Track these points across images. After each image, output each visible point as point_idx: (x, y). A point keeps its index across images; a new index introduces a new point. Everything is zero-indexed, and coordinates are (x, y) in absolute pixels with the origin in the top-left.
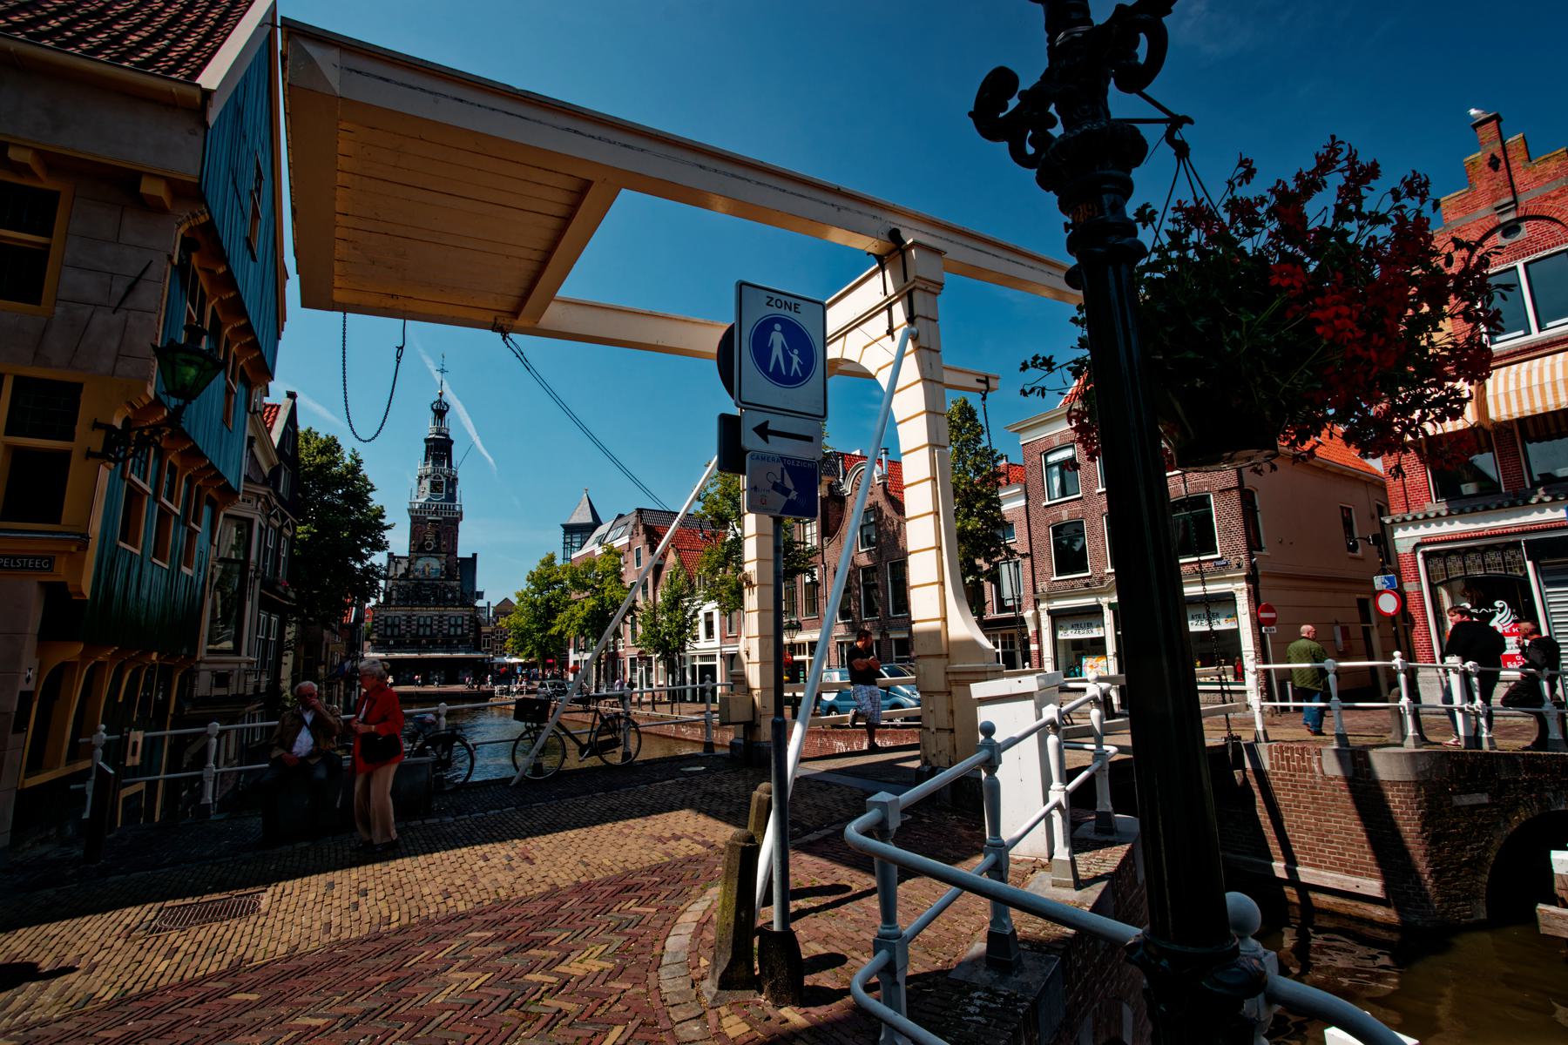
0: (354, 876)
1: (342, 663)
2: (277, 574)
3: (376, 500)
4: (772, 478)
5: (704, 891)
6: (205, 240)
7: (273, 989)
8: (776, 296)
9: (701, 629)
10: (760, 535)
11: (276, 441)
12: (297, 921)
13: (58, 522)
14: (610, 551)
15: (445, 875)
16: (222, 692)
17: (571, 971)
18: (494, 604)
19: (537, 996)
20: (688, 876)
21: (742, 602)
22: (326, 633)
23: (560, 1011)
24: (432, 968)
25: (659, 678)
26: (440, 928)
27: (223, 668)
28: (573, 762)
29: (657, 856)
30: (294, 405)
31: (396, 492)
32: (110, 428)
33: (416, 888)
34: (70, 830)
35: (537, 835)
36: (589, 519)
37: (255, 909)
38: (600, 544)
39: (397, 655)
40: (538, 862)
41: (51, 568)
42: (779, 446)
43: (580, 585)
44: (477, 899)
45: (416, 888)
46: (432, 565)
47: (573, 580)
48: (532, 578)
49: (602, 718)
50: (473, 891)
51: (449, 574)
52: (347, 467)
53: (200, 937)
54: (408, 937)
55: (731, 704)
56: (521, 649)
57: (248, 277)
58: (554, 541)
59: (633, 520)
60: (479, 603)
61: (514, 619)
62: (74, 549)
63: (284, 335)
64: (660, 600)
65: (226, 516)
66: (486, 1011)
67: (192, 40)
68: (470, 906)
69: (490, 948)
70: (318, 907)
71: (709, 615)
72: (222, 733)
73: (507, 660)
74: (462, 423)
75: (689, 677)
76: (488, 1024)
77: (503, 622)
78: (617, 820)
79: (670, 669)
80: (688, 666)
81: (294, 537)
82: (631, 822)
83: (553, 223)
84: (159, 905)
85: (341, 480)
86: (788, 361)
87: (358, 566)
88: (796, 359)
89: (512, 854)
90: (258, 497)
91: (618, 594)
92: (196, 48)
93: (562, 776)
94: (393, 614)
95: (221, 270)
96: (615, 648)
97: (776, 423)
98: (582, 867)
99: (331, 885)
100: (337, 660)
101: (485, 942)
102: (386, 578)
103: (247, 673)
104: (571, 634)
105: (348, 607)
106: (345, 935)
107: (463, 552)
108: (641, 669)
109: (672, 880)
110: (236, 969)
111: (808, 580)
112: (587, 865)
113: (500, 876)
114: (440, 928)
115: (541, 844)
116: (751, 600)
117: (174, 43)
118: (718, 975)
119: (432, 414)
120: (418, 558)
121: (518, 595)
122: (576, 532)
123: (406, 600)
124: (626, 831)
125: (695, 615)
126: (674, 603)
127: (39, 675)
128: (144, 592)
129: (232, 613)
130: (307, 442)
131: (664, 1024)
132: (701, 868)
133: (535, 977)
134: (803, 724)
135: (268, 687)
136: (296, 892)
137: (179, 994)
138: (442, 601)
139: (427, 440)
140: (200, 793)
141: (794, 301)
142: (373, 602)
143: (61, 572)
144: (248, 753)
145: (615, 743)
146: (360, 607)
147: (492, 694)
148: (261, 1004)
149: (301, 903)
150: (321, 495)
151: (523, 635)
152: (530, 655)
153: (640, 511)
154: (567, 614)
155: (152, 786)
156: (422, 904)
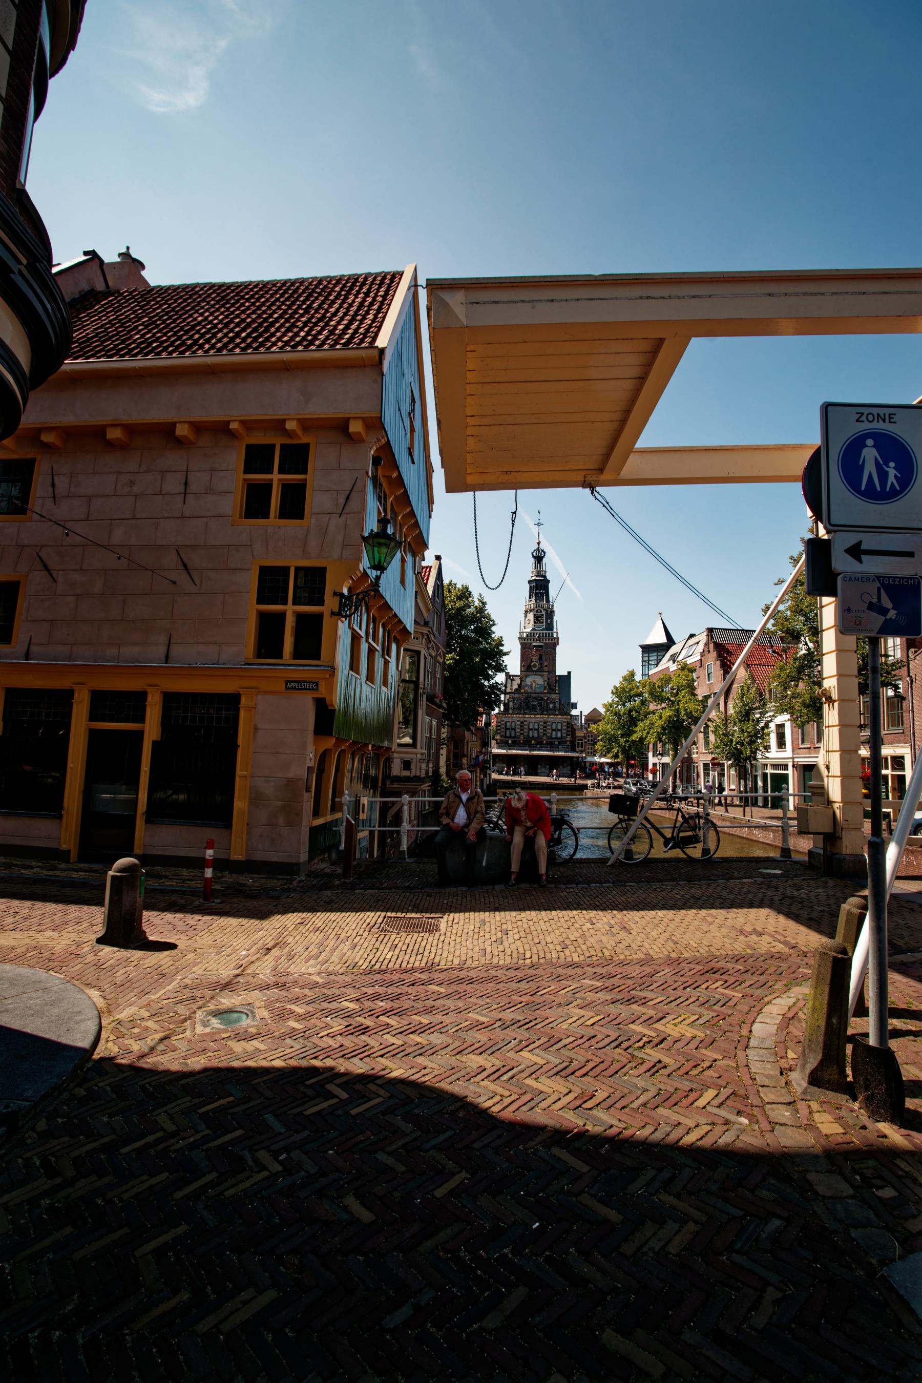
0: (498, 918)
1: (477, 757)
2: (435, 690)
3: (497, 632)
4: (867, 599)
5: (788, 987)
6: (385, 457)
7: (454, 987)
8: (866, 411)
9: (773, 739)
10: (840, 651)
11: (430, 593)
12: (464, 943)
13: (319, 659)
14: (684, 667)
15: (562, 930)
16: (406, 773)
17: (668, 1031)
18: (585, 713)
19: (640, 1044)
20: (771, 970)
21: (820, 717)
22: (467, 734)
23: (660, 1062)
24: (559, 1000)
25: (731, 785)
26: (561, 971)
27: (407, 757)
28: (660, 851)
29: (740, 946)
30: (440, 564)
31: (510, 624)
32: (341, 595)
33: (541, 936)
34: (334, 856)
35: (632, 909)
36: (663, 639)
37: (437, 929)
38: (674, 661)
39: (514, 752)
40: (634, 932)
41: (317, 690)
42: (872, 566)
43: (658, 697)
44: (587, 954)
45: (541, 936)
46: (537, 681)
47: (651, 694)
48: (616, 692)
49: (683, 816)
50: (584, 947)
51: (550, 688)
52: (476, 608)
53: (408, 941)
54: (539, 972)
55: (811, 816)
56: (609, 751)
57: (411, 475)
58: (634, 662)
59: (703, 638)
60: (574, 712)
61: (601, 726)
62: (328, 676)
63: (433, 514)
64: (731, 711)
65: (405, 650)
66: (600, 1045)
67: (371, 317)
68: (582, 958)
69: (600, 995)
70: (476, 936)
71: (780, 727)
72: (410, 802)
73: (597, 759)
74: (554, 568)
75: (760, 784)
76: (603, 1056)
77: (593, 728)
78: (701, 907)
79: (742, 775)
80: (759, 773)
81: (444, 662)
82: (713, 912)
83: (629, 385)
84: (383, 914)
85: (473, 619)
86: (883, 476)
87: (486, 683)
88: (892, 473)
89: (612, 922)
90: (423, 634)
91: (691, 706)
92: (373, 321)
93: (648, 862)
94: (510, 720)
95: (395, 475)
96: (690, 754)
97: (870, 541)
98: (671, 944)
99: (484, 922)
100: (474, 755)
101: (597, 990)
102: (505, 693)
103: (421, 761)
104: (651, 739)
105: (481, 714)
106: (495, 961)
107: (560, 671)
108: (714, 774)
109: (759, 972)
110: (430, 968)
111: (891, 693)
112: (676, 943)
113: (604, 939)
114: (561, 971)
115: (636, 918)
116: (831, 715)
117: (361, 322)
118: (808, 1071)
119: (533, 560)
120: (527, 676)
121: (605, 706)
122: (652, 651)
123: (519, 709)
124: (709, 919)
125: (767, 726)
126: (746, 715)
127: (315, 756)
128: (363, 704)
129: (410, 720)
130: (450, 592)
131: (756, 1101)
132: (784, 965)
133: (637, 1028)
134: (899, 844)
135: (433, 772)
136: (461, 923)
137: (400, 976)
138: (545, 710)
139: (530, 582)
140: (399, 844)
141: (887, 411)
142: (497, 711)
143: (323, 692)
144: (423, 817)
145: (695, 840)
146: (488, 714)
147: (585, 787)
148: (447, 996)
149: (465, 931)
150: (460, 631)
151: (611, 740)
152: (616, 756)
153: (710, 631)
154: (646, 723)
155: (372, 833)
156: (546, 949)
